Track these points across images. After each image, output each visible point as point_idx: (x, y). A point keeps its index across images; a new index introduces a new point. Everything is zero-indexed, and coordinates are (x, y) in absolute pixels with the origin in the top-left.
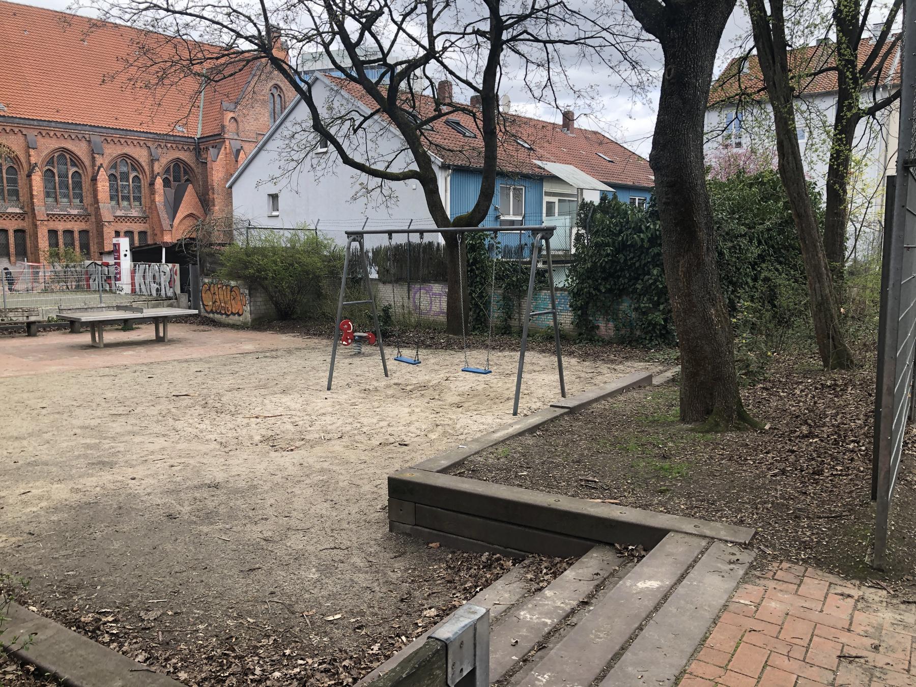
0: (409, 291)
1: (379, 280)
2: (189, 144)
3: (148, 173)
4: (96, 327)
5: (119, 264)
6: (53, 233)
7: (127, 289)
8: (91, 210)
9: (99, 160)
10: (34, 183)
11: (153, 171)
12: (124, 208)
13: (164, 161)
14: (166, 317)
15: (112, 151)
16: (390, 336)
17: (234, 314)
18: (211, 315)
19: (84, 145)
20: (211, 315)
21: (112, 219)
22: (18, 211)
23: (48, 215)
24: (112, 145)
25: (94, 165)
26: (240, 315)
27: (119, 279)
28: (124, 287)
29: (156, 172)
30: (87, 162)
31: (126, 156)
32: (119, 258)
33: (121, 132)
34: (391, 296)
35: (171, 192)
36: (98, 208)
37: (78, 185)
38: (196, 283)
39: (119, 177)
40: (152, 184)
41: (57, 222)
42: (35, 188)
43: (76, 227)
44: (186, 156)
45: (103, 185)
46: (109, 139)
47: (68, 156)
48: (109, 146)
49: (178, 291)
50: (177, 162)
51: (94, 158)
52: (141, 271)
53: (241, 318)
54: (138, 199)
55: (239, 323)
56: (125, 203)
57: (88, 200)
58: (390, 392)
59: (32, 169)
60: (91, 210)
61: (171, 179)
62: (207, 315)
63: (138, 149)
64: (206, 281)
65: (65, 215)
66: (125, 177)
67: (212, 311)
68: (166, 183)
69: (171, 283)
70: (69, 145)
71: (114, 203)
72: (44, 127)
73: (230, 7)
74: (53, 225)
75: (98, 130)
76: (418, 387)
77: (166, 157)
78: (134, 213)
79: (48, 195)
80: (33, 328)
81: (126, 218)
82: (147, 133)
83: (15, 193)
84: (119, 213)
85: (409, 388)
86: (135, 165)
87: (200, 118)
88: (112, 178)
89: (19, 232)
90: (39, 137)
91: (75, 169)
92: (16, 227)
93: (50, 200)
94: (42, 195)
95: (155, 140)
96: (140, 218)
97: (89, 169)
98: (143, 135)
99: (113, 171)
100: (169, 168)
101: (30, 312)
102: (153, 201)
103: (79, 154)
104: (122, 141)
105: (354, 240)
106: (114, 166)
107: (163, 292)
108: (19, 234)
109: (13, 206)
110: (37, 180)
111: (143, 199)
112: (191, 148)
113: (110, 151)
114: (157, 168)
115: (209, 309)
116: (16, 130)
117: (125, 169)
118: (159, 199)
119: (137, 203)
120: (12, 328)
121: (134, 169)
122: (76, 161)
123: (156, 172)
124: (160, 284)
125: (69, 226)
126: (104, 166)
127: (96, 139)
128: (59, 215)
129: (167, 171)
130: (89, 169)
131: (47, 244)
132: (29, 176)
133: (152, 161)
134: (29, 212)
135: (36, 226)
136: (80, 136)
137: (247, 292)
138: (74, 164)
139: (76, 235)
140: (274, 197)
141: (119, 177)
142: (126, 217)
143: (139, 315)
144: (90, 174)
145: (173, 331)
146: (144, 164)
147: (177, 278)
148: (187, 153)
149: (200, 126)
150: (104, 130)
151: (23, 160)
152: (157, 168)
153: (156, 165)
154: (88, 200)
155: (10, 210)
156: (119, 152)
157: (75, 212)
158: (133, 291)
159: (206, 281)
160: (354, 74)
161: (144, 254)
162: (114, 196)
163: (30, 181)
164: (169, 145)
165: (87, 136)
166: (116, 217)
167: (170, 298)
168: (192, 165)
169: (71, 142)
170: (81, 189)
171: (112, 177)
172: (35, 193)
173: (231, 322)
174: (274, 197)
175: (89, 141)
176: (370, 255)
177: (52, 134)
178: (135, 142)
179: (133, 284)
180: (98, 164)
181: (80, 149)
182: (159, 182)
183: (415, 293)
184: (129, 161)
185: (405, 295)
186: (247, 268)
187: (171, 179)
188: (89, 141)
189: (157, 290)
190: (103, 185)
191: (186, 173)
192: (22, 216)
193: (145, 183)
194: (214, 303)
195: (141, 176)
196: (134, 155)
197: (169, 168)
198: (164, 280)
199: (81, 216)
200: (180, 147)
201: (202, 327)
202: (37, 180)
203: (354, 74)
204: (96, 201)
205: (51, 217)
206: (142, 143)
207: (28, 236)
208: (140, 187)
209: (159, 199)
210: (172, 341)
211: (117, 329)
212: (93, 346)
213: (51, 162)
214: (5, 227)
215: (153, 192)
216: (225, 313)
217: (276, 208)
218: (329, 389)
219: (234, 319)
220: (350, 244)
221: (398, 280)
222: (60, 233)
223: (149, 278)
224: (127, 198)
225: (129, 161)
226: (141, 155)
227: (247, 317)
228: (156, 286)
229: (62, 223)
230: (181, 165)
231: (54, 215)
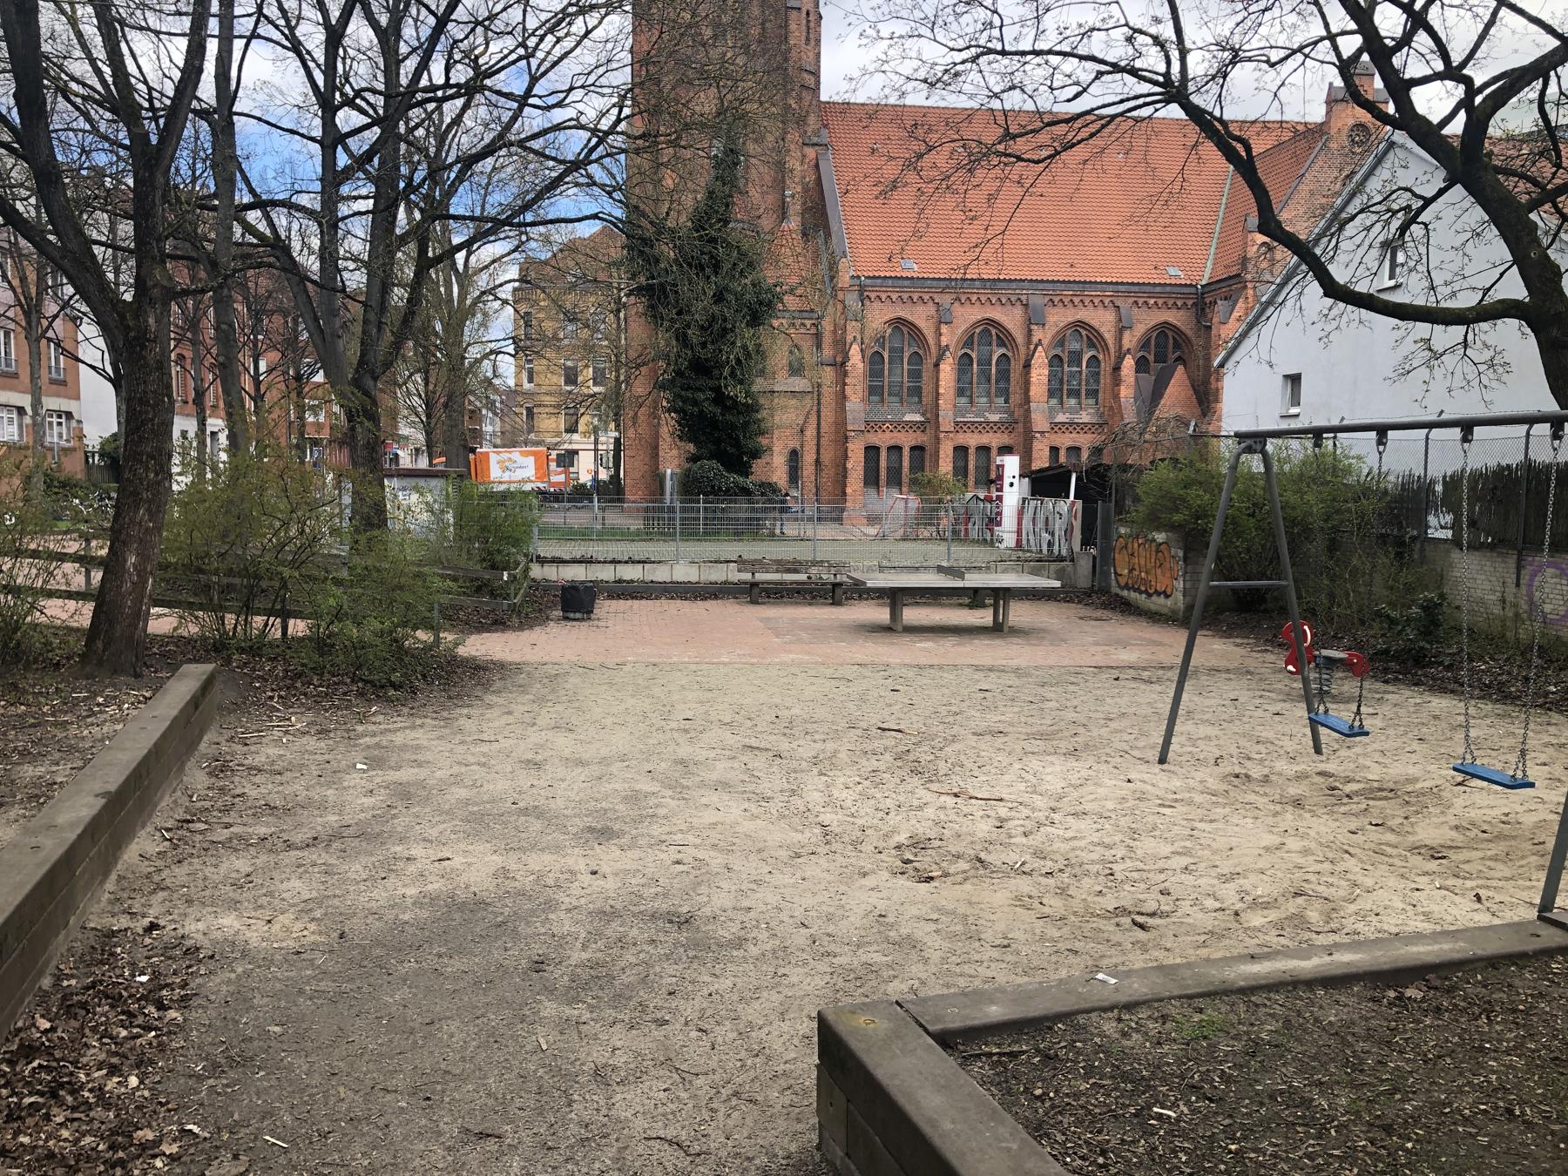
0: (1519, 568)
1: (1456, 542)
2: (1185, 296)
3: (1112, 350)
4: (896, 597)
5: (1000, 498)
6: (961, 451)
7: (1009, 540)
8: (1018, 413)
9: (1038, 333)
10: (942, 375)
11: (1121, 347)
12: (1072, 411)
13: (1140, 330)
14: (1008, 589)
15: (1058, 318)
16: (1430, 665)
17: (1158, 594)
18: (1125, 593)
19: (1018, 312)
20: (1125, 593)
21: (1046, 427)
22: (918, 418)
23: (957, 423)
24: (1060, 309)
25: (1029, 342)
26: (1167, 596)
27: (999, 524)
28: (1005, 536)
29: (1125, 348)
30: (1020, 338)
31: (1080, 325)
32: (1000, 489)
33: (1076, 287)
34: (1477, 581)
35: (1149, 379)
36: (1028, 411)
37: (1004, 375)
38: (1106, 536)
39: (1066, 359)
40: (1117, 369)
41: (969, 435)
42: (942, 383)
43: (907, 440)
44: (1173, 317)
45: (1040, 374)
46: (1056, 299)
47: (994, 332)
48: (1056, 310)
49: (1077, 547)
50: (1164, 329)
51: (1030, 331)
52: (1031, 511)
53: (1169, 602)
54: (1093, 393)
55: (1165, 611)
56: (1073, 401)
57: (1015, 398)
58: (1293, 790)
59: (942, 352)
60: (1018, 413)
61: (1151, 358)
62: (1118, 591)
63: (1101, 311)
64: (1122, 530)
65: (980, 423)
66: (1076, 358)
67: (1127, 587)
68: (1141, 365)
69: (1069, 531)
70: (997, 314)
71: (1054, 401)
72: (958, 287)
73: (1127, 25)
74: (961, 439)
75: (1041, 286)
76: (1372, 790)
77: (1145, 321)
78: (1085, 417)
79: (960, 392)
80: (839, 591)
81: (1071, 426)
82: (1117, 283)
83: (916, 391)
84: (1061, 418)
85: (1349, 788)
86: (1093, 338)
87: (1213, 250)
88: (1056, 361)
89: (918, 449)
90: (957, 304)
91: (1002, 351)
92: (913, 443)
93: (964, 400)
94: (952, 392)
95: (1128, 294)
96: (1093, 425)
97: (1022, 350)
98: (1111, 288)
99: (1058, 351)
100: (1149, 340)
101: (838, 567)
102: (1116, 397)
103: (1009, 327)
104: (1076, 300)
105: (1249, 450)
106: (1061, 343)
107: (1056, 548)
108: (872, 453)
109: (912, 412)
110: (947, 370)
111: (1101, 395)
112: (1190, 303)
113: (1055, 318)
114: (1042, 335)
115: (1123, 581)
116: (926, 297)
117: (1075, 346)
118: (1126, 392)
119: (1091, 401)
120: (818, 590)
121: (1091, 345)
122: (1005, 338)
123: (1125, 348)
124: (1053, 534)
125: (985, 439)
126: (1045, 342)
127: (1037, 300)
128: (973, 423)
129: (1145, 345)
130: (1022, 350)
131: (950, 467)
132: (937, 365)
133: (1120, 331)
134: (931, 422)
135: (938, 439)
136: (1013, 299)
137: (1181, 553)
138: (1002, 344)
139: (906, 452)
140: (1294, 380)
141: (1066, 359)
142: (1071, 424)
143: (959, 584)
144: (1023, 357)
145: (1019, 613)
146: (1107, 336)
147: (1077, 524)
148: (1182, 312)
149: (1209, 264)
150: (1050, 286)
151: (931, 341)
152: (1129, 341)
153: (1127, 335)
154: (1015, 398)
155: (908, 418)
156: (1071, 319)
157: (995, 417)
158: (1019, 542)
159: (1122, 530)
160: (1391, 109)
161: (1045, 484)
162: (1055, 390)
163: (938, 372)
164: (1152, 301)
165: (1024, 298)
166: (1056, 424)
167: (1060, 559)
168: (1189, 333)
169: (999, 308)
170: (1008, 380)
171: (1055, 361)
172: (941, 391)
173: (1153, 608)
174: (1294, 380)
175: (1026, 305)
176: (1439, 488)
177: (974, 298)
178: (1096, 301)
179: (1019, 532)
180: (1035, 340)
181: (1011, 319)
182: (1129, 363)
183: (1534, 575)
184: (1084, 333)
185: (1511, 579)
186: (1177, 510)
187: (1151, 358)
188: (1026, 305)
189: (1050, 544)
190: (1040, 374)
191: (1177, 346)
192: (921, 427)
193: (1106, 367)
194: (1131, 571)
195: (1101, 357)
196: (1092, 323)
197: (1149, 340)
198: (1059, 526)
199: (1003, 423)
200: (1170, 302)
201: (1099, 613)
202: (947, 370)
203: (1391, 109)
204: (1027, 400)
205: (1056, 427)
206: (1107, 301)
207: (927, 456)
208: (1098, 374)
209: (1126, 392)
210: (1015, 632)
211: (961, 605)
212: (890, 629)
213: (969, 343)
214: (899, 443)
215: (1117, 381)
216: (1146, 592)
217: (1295, 400)
218: (1162, 761)
219: (1158, 603)
220: (1239, 455)
221: (1499, 545)
222: (972, 451)
223: (1040, 525)
224: (1074, 393)
225: (1084, 333)
226: (1103, 321)
227: (1178, 601)
228: (1046, 536)
229: (976, 436)
230: (1170, 334)
231: (965, 423)
